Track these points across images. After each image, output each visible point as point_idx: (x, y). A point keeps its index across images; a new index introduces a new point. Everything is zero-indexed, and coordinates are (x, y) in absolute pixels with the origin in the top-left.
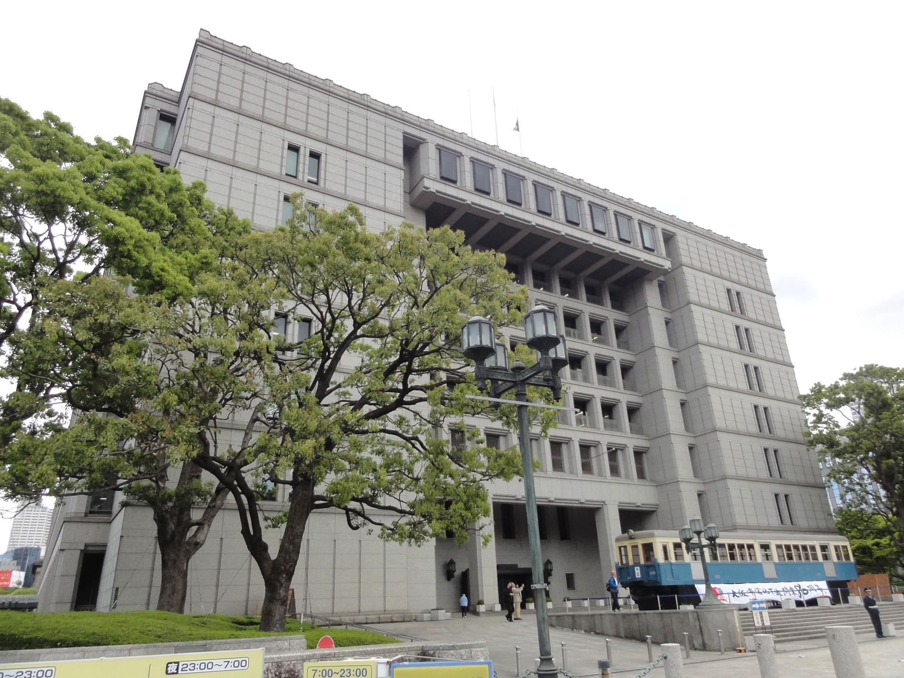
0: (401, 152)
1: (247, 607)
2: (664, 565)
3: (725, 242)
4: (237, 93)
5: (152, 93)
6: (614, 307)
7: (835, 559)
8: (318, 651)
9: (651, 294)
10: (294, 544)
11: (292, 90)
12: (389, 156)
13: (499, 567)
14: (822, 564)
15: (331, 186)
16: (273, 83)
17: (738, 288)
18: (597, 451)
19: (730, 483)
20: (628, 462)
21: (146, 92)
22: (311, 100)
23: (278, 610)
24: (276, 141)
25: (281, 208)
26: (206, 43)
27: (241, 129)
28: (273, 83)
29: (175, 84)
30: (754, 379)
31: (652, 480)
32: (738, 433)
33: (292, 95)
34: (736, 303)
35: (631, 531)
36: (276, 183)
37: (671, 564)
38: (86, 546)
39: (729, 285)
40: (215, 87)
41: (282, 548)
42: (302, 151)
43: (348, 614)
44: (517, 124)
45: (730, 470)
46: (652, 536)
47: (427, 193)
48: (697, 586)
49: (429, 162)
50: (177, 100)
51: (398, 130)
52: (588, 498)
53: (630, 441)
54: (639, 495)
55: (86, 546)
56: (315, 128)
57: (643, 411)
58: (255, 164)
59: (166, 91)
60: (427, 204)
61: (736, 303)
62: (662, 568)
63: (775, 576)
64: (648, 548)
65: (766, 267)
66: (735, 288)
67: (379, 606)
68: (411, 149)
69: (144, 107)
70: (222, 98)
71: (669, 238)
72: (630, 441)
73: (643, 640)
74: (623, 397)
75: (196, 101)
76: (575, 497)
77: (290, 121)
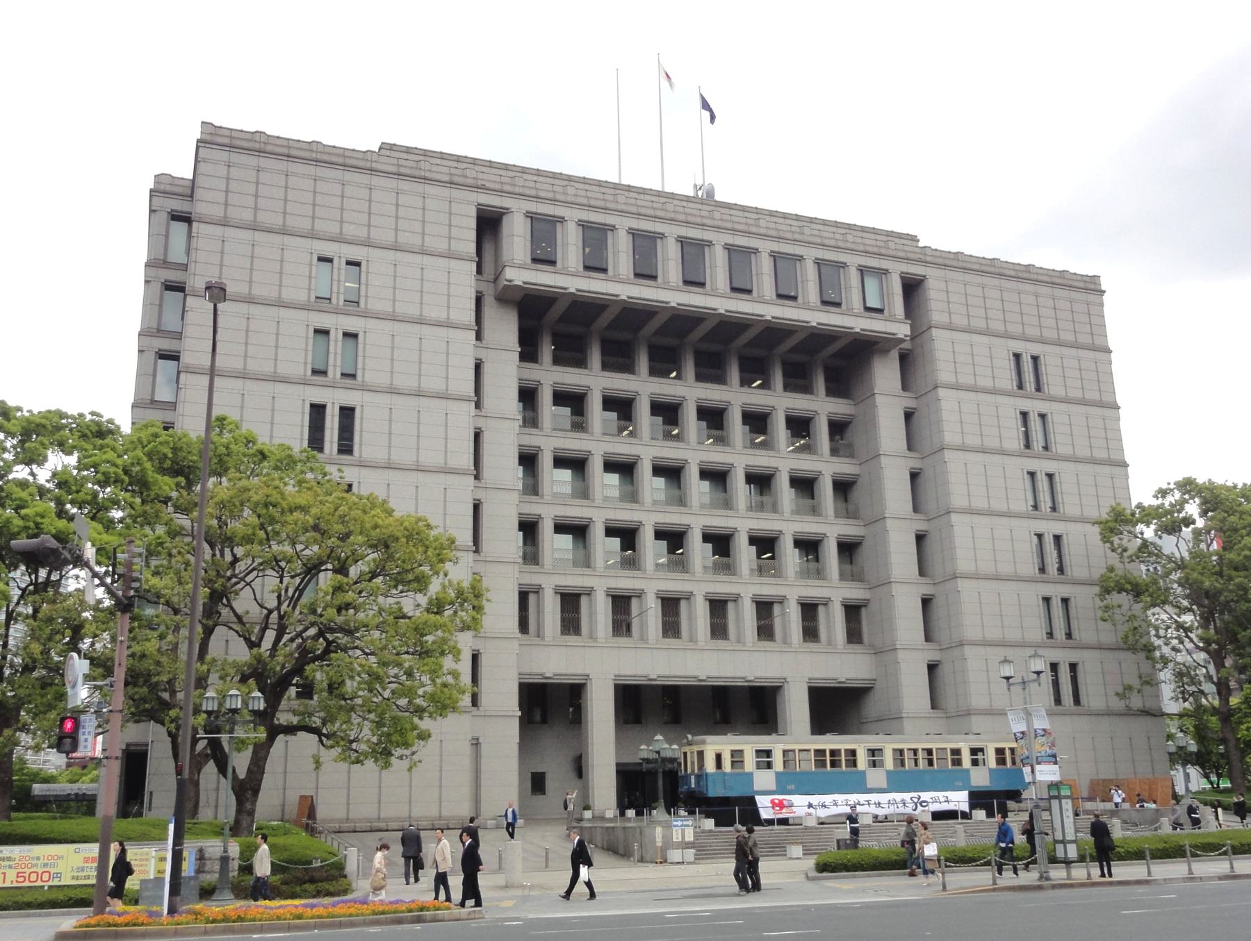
0: (473, 223)
1: (283, 811)
2: (713, 774)
3: (1027, 275)
4: (250, 201)
5: (163, 189)
6: (831, 392)
7: (992, 763)
8: (825, 874)
9: (884, 374)
10: (259, 767)
11: (321, 179)
12: (455, 246)
13: (618, 765)
14: (968, 771)
15: (374, 305)
16: (296, 175)
17: (1036, 349)
18: (783, 609)
19: (968, 651)
20: (834, 622)
21: (151, 191)
22: (346, 187)
23: (245, 822)
24: (301, 252)
25: (310, 348)
26: (213, 140)
27: (258, 250)
28: (296, 175)
29: (184, 169)
30: (1044, 492)
31: (872, 646)
32: (997, 578)
33: (322, 187)
34: (1028, 373)
35: (690, 736)
36: (302, 315)
37: (725, 774)
38: (128, 745)
39: (1018, 346)
40: (222, 200)
41: (249, 771)
42: (336, 261)
43: (397, 819)
44: (705, 105)
45: (971, 633)
46: (704, 742)
47: (511, 288)
48: (757, 798)
49: (516, 239)
50: (189, 192)
51: (469, 203)
52: (759, 675)
53: (834, 589)
54: (840, 665)
55: (128, 745)
56: (352, 227)
57: (866, 545)
58: (275, 295)
59: (177, 182)
60: (518, 297)
61: (1028, 373)
62: (710, 779)
63: (885, 786)
64: (701, 754)
65: (1102, 305)
66: (1027, 349)
67: (434, 812)
68: (489, 225)
69: (152, 211)
70: (233, 213)
71: (912, 288)
72: (834, 589)
73: (1143, 858)
74: (830, 527)
75: (202, 225)
76: (739, 674)
77: (319, 225)
